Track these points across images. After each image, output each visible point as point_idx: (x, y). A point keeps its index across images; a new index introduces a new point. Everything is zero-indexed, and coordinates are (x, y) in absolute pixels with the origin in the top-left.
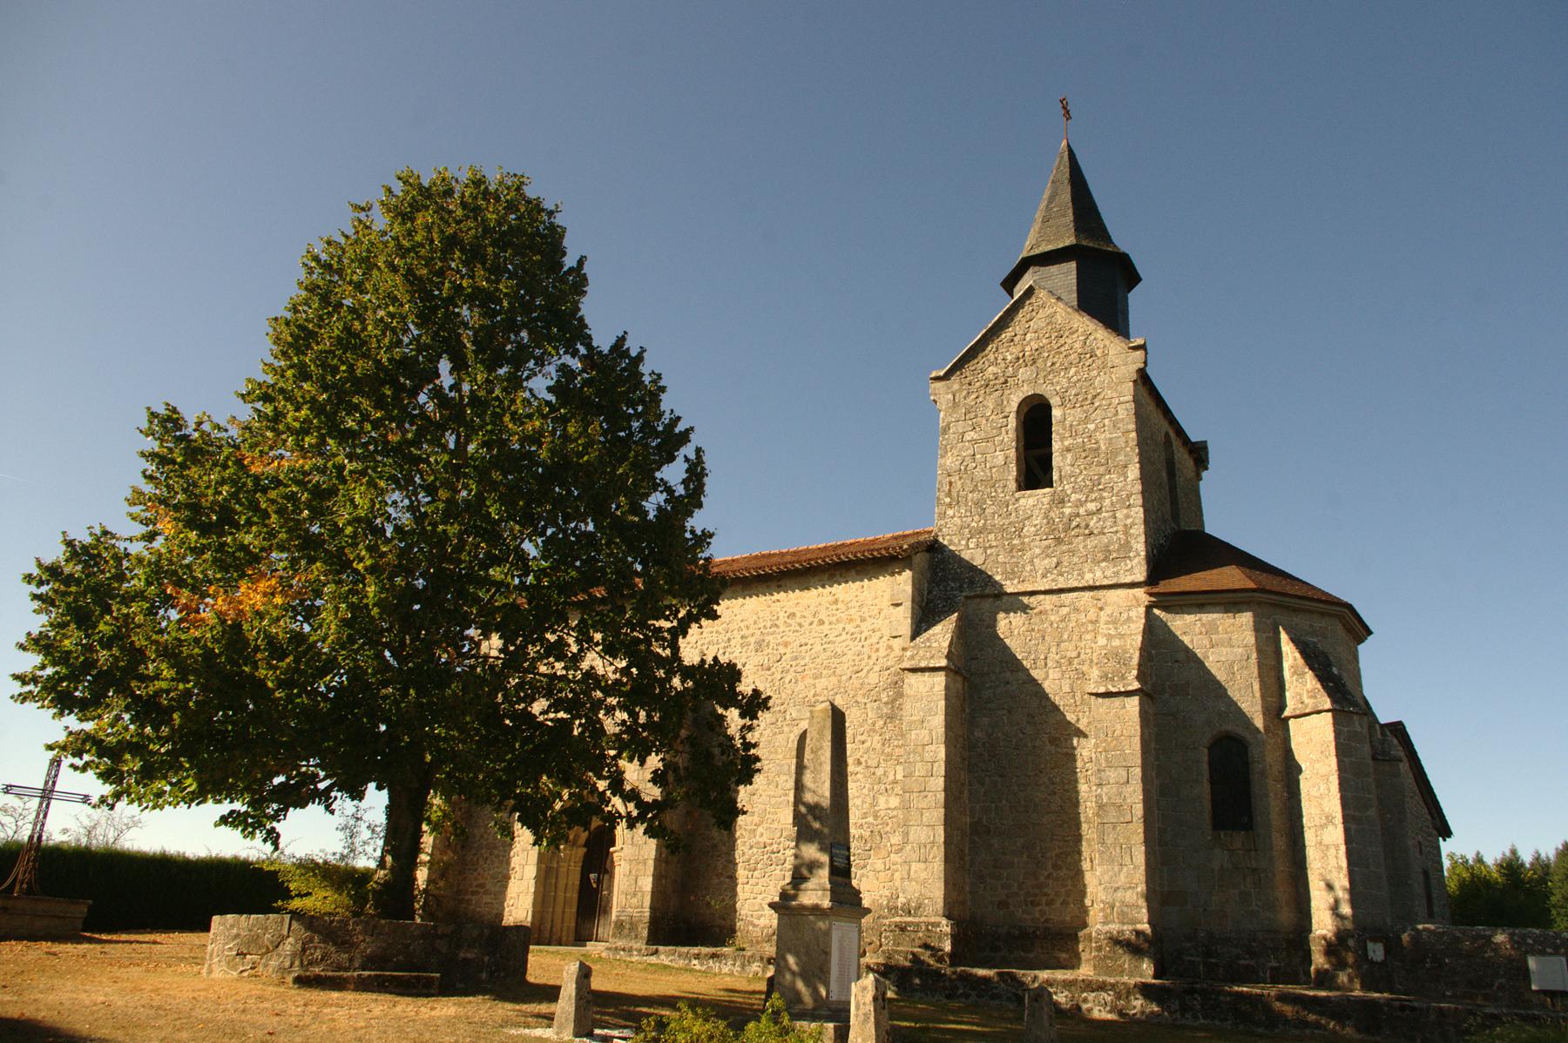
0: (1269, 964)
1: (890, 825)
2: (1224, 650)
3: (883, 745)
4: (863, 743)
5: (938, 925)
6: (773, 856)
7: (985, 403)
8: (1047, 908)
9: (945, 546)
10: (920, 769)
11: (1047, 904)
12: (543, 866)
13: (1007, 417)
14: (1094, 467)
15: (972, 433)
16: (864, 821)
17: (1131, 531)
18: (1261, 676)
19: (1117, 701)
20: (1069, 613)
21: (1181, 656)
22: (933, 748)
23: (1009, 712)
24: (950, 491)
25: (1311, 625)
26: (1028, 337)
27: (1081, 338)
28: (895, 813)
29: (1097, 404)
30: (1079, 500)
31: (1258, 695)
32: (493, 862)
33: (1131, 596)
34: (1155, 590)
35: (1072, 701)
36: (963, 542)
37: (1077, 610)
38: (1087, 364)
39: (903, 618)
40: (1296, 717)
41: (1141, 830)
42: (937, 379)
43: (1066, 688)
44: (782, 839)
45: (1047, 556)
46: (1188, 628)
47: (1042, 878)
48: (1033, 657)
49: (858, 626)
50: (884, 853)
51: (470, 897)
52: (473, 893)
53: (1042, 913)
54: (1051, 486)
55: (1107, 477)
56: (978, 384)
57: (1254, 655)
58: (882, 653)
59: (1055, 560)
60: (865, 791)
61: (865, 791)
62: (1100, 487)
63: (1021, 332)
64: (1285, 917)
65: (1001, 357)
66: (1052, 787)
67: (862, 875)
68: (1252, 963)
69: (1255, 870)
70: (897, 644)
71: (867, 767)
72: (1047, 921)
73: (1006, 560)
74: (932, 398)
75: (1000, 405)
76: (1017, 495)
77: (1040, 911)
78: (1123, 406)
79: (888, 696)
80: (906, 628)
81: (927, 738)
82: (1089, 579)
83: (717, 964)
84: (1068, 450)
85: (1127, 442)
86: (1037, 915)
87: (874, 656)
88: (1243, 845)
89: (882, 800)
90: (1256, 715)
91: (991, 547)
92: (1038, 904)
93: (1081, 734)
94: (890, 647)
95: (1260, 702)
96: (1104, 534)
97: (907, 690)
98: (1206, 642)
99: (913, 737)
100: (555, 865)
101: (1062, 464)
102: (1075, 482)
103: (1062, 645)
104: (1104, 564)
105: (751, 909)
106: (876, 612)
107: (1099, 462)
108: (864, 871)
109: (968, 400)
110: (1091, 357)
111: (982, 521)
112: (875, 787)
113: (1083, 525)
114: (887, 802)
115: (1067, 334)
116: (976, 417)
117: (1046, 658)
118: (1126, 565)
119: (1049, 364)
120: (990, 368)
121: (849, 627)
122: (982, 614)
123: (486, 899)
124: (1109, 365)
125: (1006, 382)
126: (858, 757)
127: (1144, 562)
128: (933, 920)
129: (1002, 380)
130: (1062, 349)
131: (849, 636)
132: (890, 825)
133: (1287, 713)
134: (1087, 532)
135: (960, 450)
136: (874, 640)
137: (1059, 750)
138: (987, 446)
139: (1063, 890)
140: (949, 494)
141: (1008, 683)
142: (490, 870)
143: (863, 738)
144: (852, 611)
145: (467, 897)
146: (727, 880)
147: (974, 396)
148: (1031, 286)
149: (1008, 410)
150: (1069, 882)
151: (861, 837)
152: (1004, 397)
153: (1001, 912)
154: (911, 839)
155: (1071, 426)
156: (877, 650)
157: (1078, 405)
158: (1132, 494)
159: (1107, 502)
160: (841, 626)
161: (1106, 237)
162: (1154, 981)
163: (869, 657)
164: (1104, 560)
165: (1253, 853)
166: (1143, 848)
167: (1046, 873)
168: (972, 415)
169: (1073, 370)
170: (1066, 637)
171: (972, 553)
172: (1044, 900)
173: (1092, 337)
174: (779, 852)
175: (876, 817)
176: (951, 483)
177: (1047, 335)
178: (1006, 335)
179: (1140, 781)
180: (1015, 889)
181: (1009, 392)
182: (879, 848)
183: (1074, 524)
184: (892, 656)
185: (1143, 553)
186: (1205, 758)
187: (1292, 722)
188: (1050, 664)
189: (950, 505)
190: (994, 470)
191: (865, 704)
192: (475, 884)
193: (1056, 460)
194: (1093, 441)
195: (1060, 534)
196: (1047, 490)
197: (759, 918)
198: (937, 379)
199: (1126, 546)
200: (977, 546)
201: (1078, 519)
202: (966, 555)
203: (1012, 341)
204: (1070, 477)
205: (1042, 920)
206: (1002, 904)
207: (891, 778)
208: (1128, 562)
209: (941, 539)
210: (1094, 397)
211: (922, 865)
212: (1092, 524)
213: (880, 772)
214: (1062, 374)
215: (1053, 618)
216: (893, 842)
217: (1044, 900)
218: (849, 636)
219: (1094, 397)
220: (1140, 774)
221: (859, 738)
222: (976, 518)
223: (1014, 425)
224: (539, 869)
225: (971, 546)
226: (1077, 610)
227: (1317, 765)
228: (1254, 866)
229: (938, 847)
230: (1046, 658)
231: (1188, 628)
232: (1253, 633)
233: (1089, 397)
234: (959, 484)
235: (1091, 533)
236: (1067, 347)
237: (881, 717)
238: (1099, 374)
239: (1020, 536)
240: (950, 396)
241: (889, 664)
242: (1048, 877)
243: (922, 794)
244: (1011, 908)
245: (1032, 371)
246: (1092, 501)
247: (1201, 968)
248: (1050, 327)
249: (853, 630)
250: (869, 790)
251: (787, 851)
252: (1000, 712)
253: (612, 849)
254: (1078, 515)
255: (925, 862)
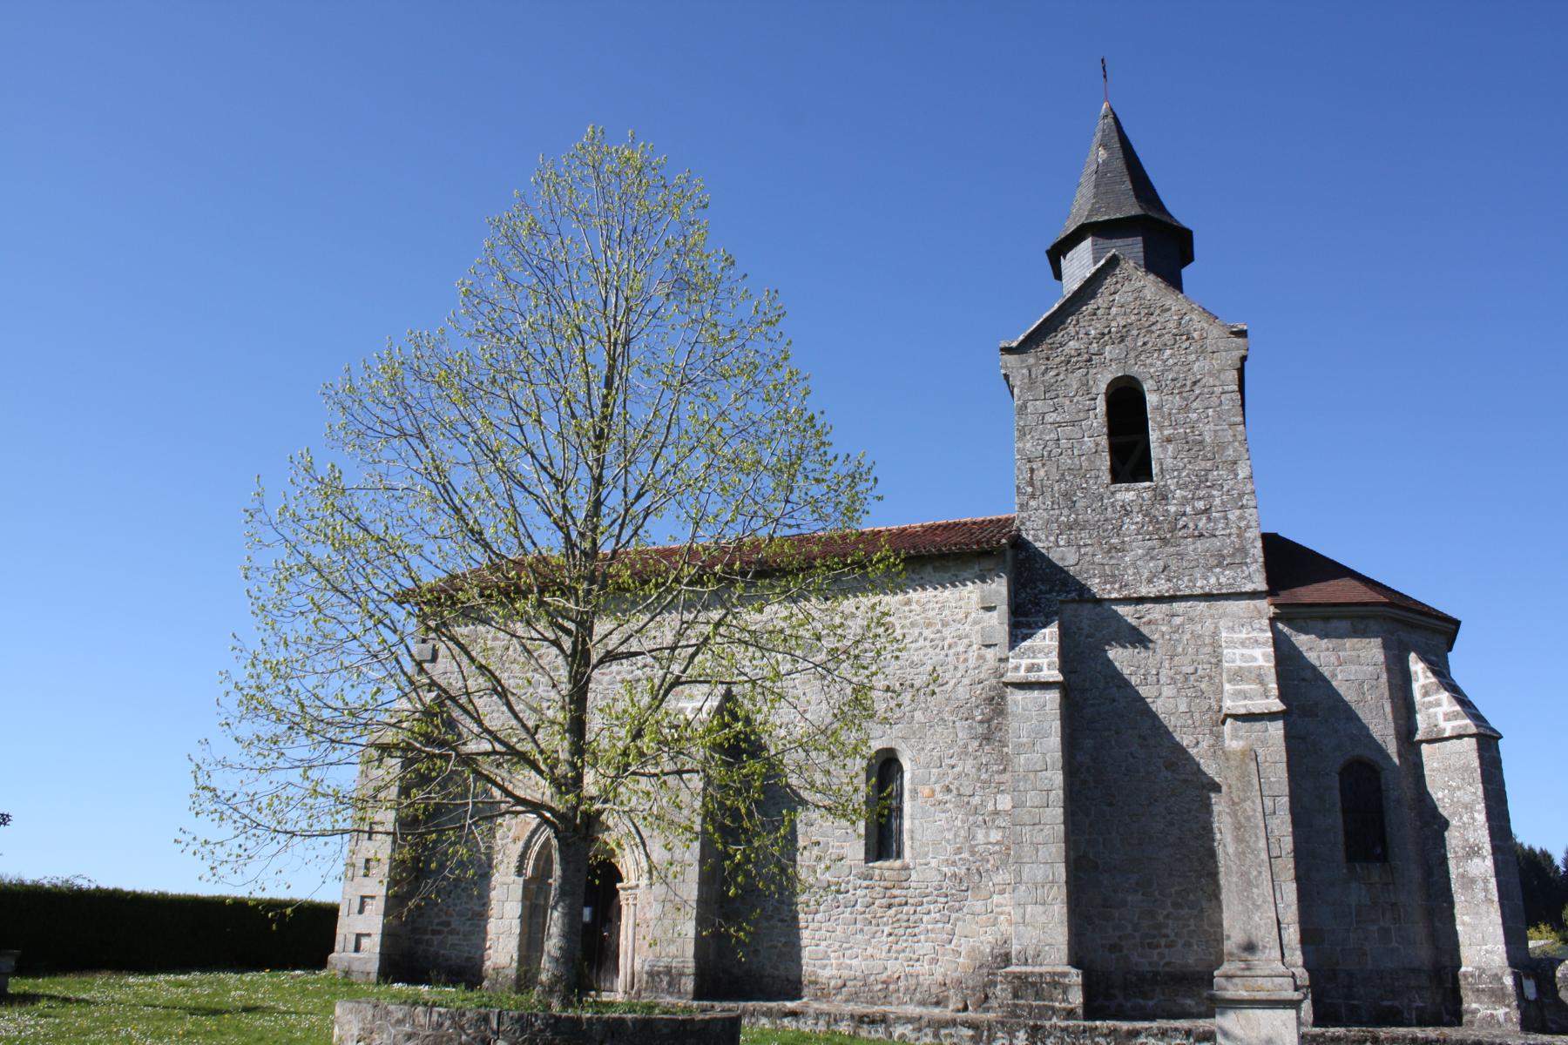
0: (1415, 1005)
1: (992, 862)
2: (1353, 668)
3: (979, 770)
4: (953, 767)
5: (1065, 975)
6: (841, 896)
7: (1067, 381)
8: (1167, 950)
9: (1030, 543)
10: (1032, 798)
11: (1166, 946)
12: (528, 903)
13: (1095, 399)
14: (1199, 461)
15: (1055, 415)
16: (957, 857)
17: (1247, 535)
18: (1392, 697)
19: (1258, 725)
20: (1182, 624)
21: (1308, 674)
22: (1049, 774)
23: (1117, 733)
24: (1031, 478)
25: (1426, 643)
26: (1114, 310)
27: (1175, 317)
28: (997, 848)
29: (1197, 392)
30: (1184, 497)
31: (1390, 717)
32: (459, 897)
33: (1252, 607)
34: (1279, 600)
35: (1190, 722)
36: (1052, 539)
37: (1191, 620)
38: (1184, 346)
39: (998, 622)
40: (1430, 741)
41: (1291, 865)
42: (1008, 351)
43: (1183, 708)
44: (851, 878)
45: (1152, 558)
46: (1314, 649)
47: (1161, 918)
48: (1142, 671)
49: (938, 631)
50: (984, 893)
51: (429, 936)
52: (434, 932)
53: (1161, 955)
54: (1151, 480)
55: (1215, 473)
56: (1058, 360)
57: (1384, 676)
58: (972, 663)
59: (1161, 563)
60: (958, 823)
61: (958, 823)
62: (1208, 484)
63: (1105, 305)
64: (1422, 954)
65: (1083, 331)
66: (1169, 817)
67: (958, 919)
68: (1397, 1003)
69: (1393, 905)
70: (990, 654)
71: (959, 795)
72: (1168, 964)
73: (1105, 561)
74: (1003, 372)
75: (1085, 386)
76: (1112, 488)
77: (1159, 953)
78: (1228, 396)
79: (983, 714)
80: (1002, 633)
81: (1040, 763)
82: (1201, 586)
83: (794, 1023)
84: (1169, 441)
85: (1235, 435)
86: (1156, 958)
87: (962, 667)
88: (1381, 878)
89: (980, 835)
90: (1388, 739)
91: (1085, 545)
92: (1158, 946)
93: (1217, 788)
94: (981, 657)
95: (1392, 725)
96: (1215, 536)
97: (1010, 707)
98: (1333, 659)
99: (1022, 762)
100: (542, 902)
101: (1162, 456)
102: (1179, 476)
103: (1176, 658)
104: (1218, 570)
105: (814, 956)
106: (962, 616)
107: (1204, 456)
108: (959, 915)
109: (1046, 377)
110: (1188, 339)
111: (1073, 516)
112: (971, 818)
113: (1191, 525)
114: (987, 835)
115: (1158, 312)
116: (1057, 396)
117: (1158, 674)
118: (1243, 572)
119: (1140, 344)
120: (1071, 343)
121: (926, 633)
122: (1081, 621)
123: (452, 939)
124: (1209, 349)
125: (1090, 360)
126: (947, 783)
127: (1263, 570)
128: (1059, 969)
129: (1086, 357)
130: (1154, 328)
131: (927, 643)
132: (992, 862)
133: (1418, 737)
134: (1196, 533)
135: (1042, 433)
136: (961, 649)
137: (1177, 776)
138: (1072, 430)
139: (1185, 931)
140: (1031, 483)
141: (1114, 701)
142: (456, 905)
143: (952, 762)
144: (931, 614)
145: (426, 937)
146: (779, 924)
147: (1053, 373)
148: (1114, 256)
149: (1094, 391)
150: (1192, 922)
151: (955, 875)
152: (1089, 376)
153: (1113, 956)
154: (1025, 877)
155: (1170, 414)
156: (966, 660)
157: (1176, 391)
158: (1244, 494)
159: (1217, 501)
160: (916, 631)
161: (1160, 207)
162: (1318, 1030)
163: (956, 668)
164: (1217, 566)
165: (1391, 887)
166: (1295, 885)
167: (1165, 913)
168: (1052, 394)
169: (1168, 352)
170: (1180, 650)
171: (1064, 555)
172: (1163, 942)
173: (1187, 318)
174: (847, 892)
175: (973, 853)
176: (1032, 470)
177: (1136, 311)
178: (1088, 309)
179: (1288, 812)
180: (1129, 930)
181: (1095, 371)
182: (978, 887)
183: (1181, 523)
184: (985, 668)
185: (1261, 560)
186: (1337, 785)
187: (1424, 747)
188: (1163, 679)
189: (1033, 496)
190: (1083, 458)
191: (954, 722)
192: (436, 921)
193: (1155, 451)
194: (1197, 433)
195: (1167, 533)
196: (1147, 484)
197: (824, 967)
198: (1008, 351)
199: (1243, 550)
200: (1069, 544)
201: (1184, 518)
202: (1054, 556)
203: (1095, 314)
204: (1174, 471)
205: (1162, 963)
206: (1114, 948)
207: (990, 807)
208: (1245, 568)
209: (1024, 534)
210: (1195, 383)
211: (1040, 909)
212: (1201, 525)
213: (976, 800)
214: (1156, 355)
215: (1164, 629)
216: (995, 881)
217: (1163, 942)
218: (928, 643)
219: (1195, 383)
220: (1288, 804)
221: (948, 761)
222: (1066, 512)
223: (1104, 408)
224: (524, 907)
225: (1062, 543)
226: (1191, 620)
227: (1458, 793)
228: (1393, 901)
229: (1059, 888)
230: (1158, 674)
231: (1314, 649)
232: (1382, 650)
233: (1189, 383)
234: (1042, 473)
235: (1201, 535)
236: (1159, 326)
237: (975, 738)
238: (1197, 359)
239: (1118, 535)
240: (1025, 371)
241: (982, 676)
242: (1167, 916)
243: (1037, 827)
244: (1125, 951)
245: (1121, 349)
246: (1200, 499)
247: (1343, 1010)
248: (1138, 303)
249: (932, 636)
250: (963, 822)
251: (858, 892)
252: (1107, 733)
253: (619, 885)
254: (1184, 514)
255: (1044, 904)
